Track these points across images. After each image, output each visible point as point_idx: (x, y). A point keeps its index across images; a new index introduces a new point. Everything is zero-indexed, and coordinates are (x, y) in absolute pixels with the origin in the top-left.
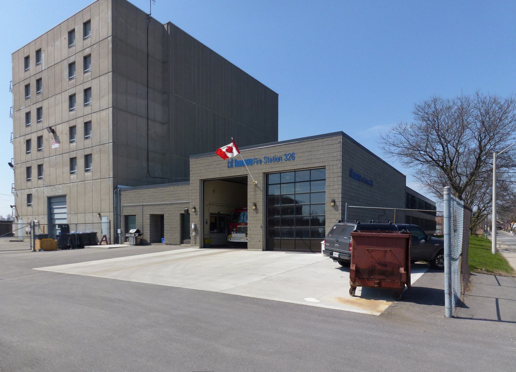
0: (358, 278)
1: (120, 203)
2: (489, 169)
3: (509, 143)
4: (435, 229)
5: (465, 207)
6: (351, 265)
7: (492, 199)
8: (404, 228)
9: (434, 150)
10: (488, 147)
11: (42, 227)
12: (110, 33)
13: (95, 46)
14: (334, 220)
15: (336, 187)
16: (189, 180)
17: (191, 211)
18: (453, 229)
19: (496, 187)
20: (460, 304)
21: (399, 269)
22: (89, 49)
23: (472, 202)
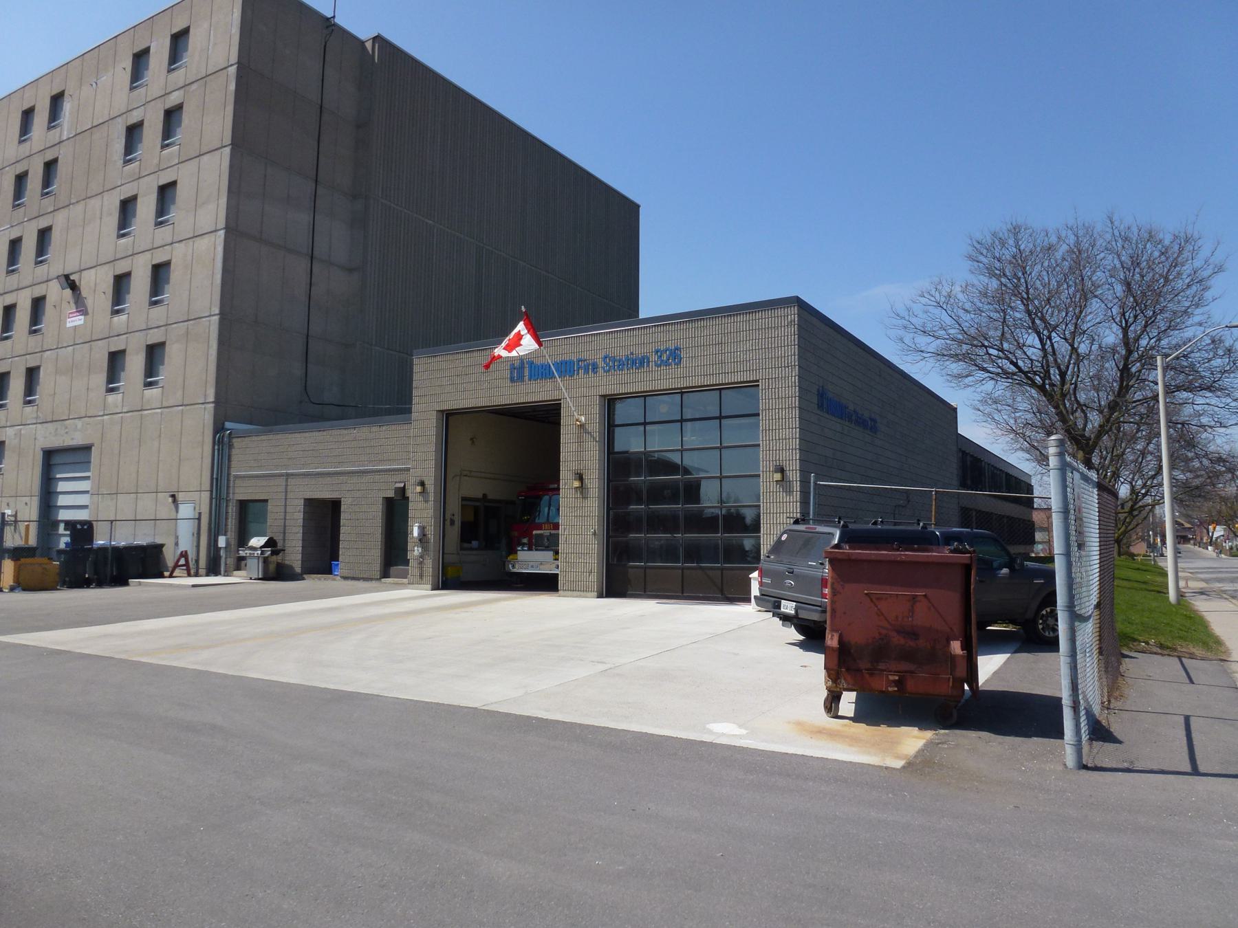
0: (844, 669)
1: (229, 468)
2: (1150, 395)
3: (1188, 333)
4: (1032, 541)
5: (1101, 487)
6: (828, 636)
7: (1161, 468)
8: (958, 538)
9: (1020, 347)
10: (1143, 342)
11: (22, 526)
12: (234, 58)
13: (194, 87)
14: (783, 518)
15: (786, 433)
16: (409, 411)
17: (413, 492)
18: (1074, 542)
19: (1169, 437)
20: (1100, 733)
21: (949, 644)
22: (182, 92)
23: (1116, 475)
